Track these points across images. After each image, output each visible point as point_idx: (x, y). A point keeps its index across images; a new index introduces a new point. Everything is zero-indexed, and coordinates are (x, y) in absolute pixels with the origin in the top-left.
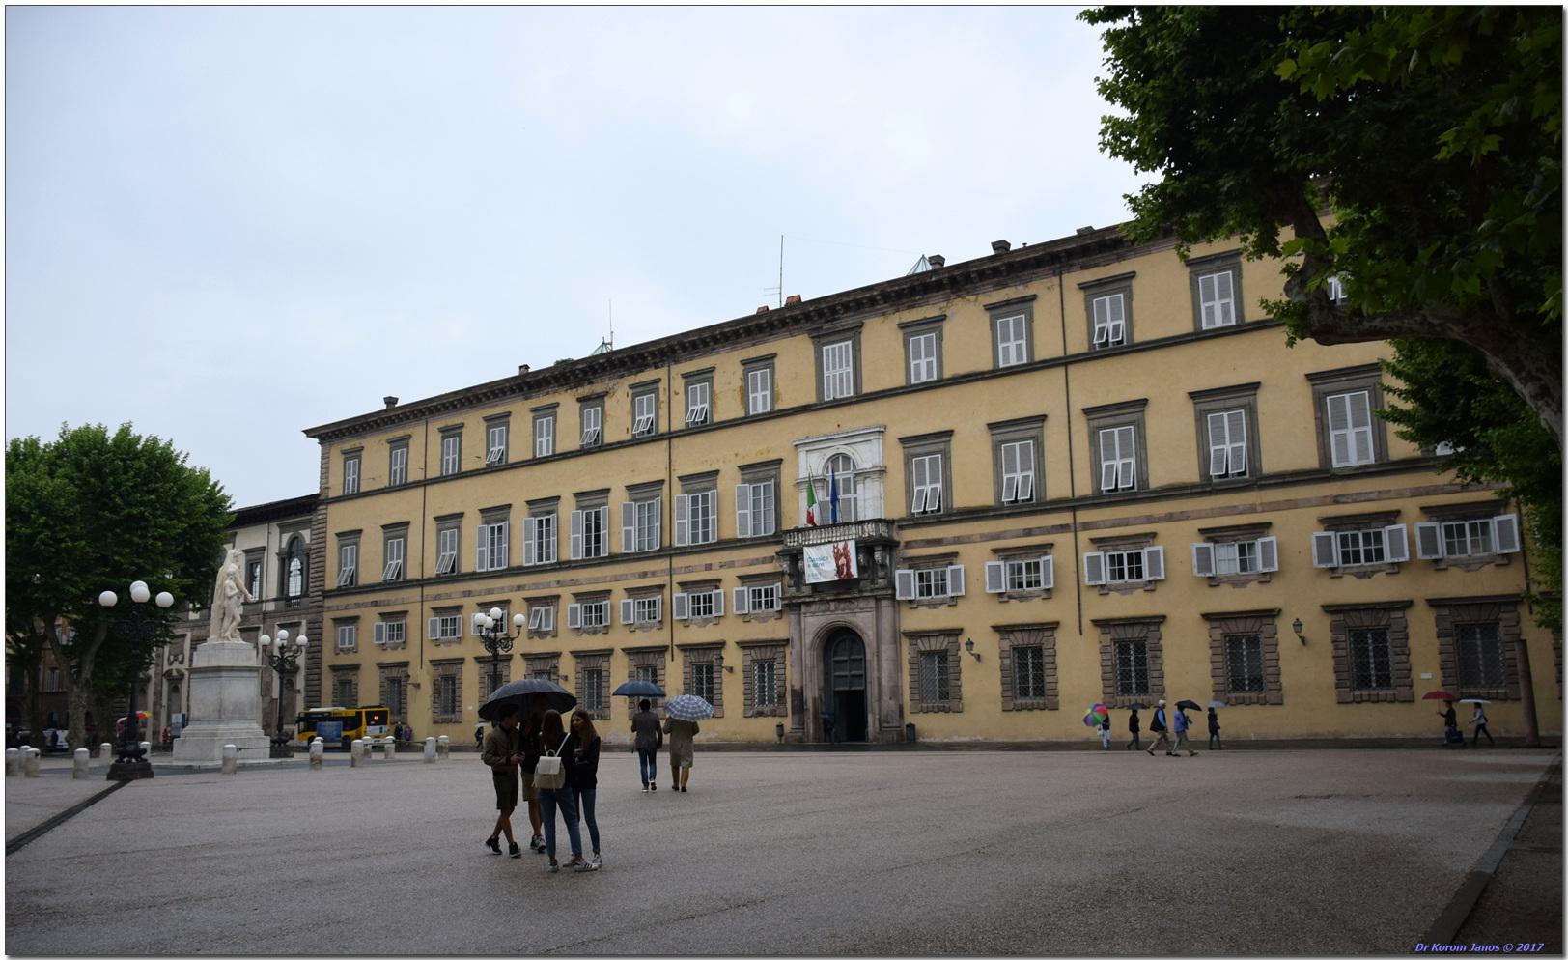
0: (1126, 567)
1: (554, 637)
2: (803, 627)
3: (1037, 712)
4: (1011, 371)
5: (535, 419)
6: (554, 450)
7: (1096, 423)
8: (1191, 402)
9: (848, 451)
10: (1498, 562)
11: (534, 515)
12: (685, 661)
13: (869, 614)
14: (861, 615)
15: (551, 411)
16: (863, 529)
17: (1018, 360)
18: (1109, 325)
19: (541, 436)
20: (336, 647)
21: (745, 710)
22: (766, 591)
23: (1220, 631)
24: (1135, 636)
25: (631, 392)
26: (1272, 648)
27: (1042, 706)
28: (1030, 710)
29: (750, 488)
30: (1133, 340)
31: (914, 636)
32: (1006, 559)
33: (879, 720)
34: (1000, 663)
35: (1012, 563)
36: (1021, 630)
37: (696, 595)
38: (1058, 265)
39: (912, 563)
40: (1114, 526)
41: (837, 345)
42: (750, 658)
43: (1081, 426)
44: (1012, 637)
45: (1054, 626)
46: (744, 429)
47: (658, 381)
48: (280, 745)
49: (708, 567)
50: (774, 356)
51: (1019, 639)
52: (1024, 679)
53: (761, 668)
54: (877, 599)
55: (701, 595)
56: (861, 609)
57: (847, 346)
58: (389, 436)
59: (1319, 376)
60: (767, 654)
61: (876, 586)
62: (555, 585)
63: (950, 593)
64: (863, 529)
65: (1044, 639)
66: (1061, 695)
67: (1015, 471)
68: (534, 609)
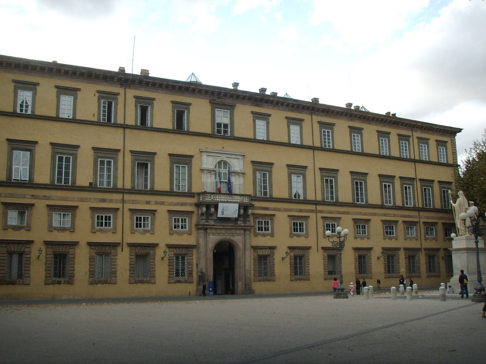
2: (208, 239)
3: (302, 281)
4: (295, 146)
6: (33, 111)
7: (323, 174)
9: (228, 160)
13: (241, 237)
22: (106, 217)
24: (19, 250)
25: (97, 95)
28: (300, 280)
31: (255, 248)
35: (294, 222)
36: (298, 249)
40: (328, 213)
43: (318, 173)
44: (294, 251)
45: (308, 248)
46: (377, 160)
47: (117, 94)
49: (148, 203)
51: (297, 252)
53: (177, 259)
54: (245, 230)
56: (238, 234)
59: (302, 167)
60: (184, 251)
62: (30, 197)
65: (306, 253)
66: (310, 275)
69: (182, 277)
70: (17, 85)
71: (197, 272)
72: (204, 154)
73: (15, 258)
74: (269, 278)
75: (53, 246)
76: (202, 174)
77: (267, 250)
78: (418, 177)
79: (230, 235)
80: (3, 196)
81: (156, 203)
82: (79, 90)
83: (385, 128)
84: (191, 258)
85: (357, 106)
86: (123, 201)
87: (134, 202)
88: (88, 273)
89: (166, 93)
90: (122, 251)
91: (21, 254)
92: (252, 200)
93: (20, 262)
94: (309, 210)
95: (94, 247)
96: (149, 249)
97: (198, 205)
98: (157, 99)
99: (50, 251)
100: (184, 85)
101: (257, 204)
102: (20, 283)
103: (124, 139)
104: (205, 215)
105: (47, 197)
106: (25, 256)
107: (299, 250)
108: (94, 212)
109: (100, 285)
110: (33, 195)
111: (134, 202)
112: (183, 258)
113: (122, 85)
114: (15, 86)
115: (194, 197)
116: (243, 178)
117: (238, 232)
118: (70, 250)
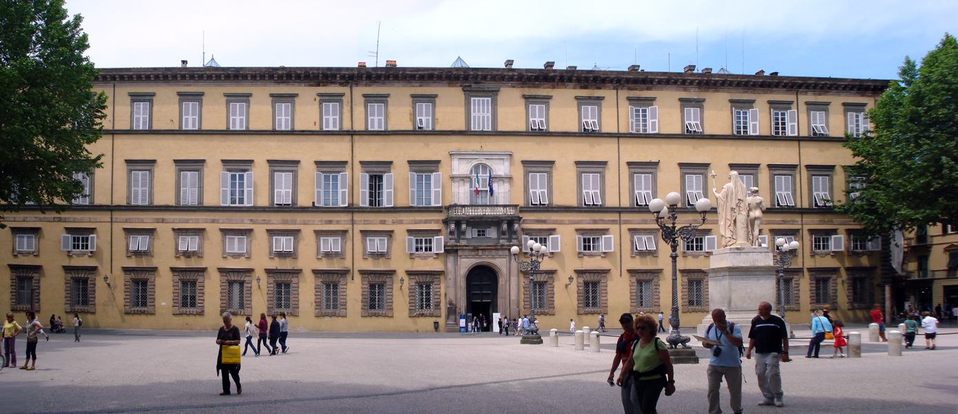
4: (303, 133)
6: (247, 127)
7: (633, 170)
8: (268, 165)
9: (488, 163)
13: (505, 259)
14: (499, 259)
20: (14, 250)
22: (83, 238)
23: (414, 281)
25: (318, 99)
27: (195, 313)
28: (592, 314)
29: (229, 174)
30: (152, 127)
32: (583, 234)
41: (481, 99)
43: (625, 170)
44: (584, 276)
47: (342, 95)
48: (532, 334)
49: (383, 222)
50: (436, 96)
51: (588, 277)
52: (587, 298)
53: (421, 287)
55: (81, 237)
57: (488, 101)
58: (685, 95)
61: (458, 244)
70: (230, 98)
71: (446, 303)
73: (236, 288)
78: (804, 163)
80: (221, 221)
81: (393, 223)
82: (296, 95)
83: (747, 94)
84: (438, 286)
85: (707, 69)
86: (353, 222)
87: (366, 222)
88: (314, 304)
89: (404, 86)
91: (242, 284)
92: (521, 211)
93: (241, 292)
95: (320, 276)
96: (385, 277)
97: (446, 222)
98: (158, 93)
99: (272, 280)
100: (426, 73)
101: (526, 216)
103: (352, 148)
104: (507, 233)
106: (245, 285)
107: (592, 275)
109: (327, 319)
111: (366, 222)
112: (428, 287)
113: (341, 84)
114: (227, 100)
115: (441, 212)
116: (510, 184)
117: (500, 253)
118: (387, 280)
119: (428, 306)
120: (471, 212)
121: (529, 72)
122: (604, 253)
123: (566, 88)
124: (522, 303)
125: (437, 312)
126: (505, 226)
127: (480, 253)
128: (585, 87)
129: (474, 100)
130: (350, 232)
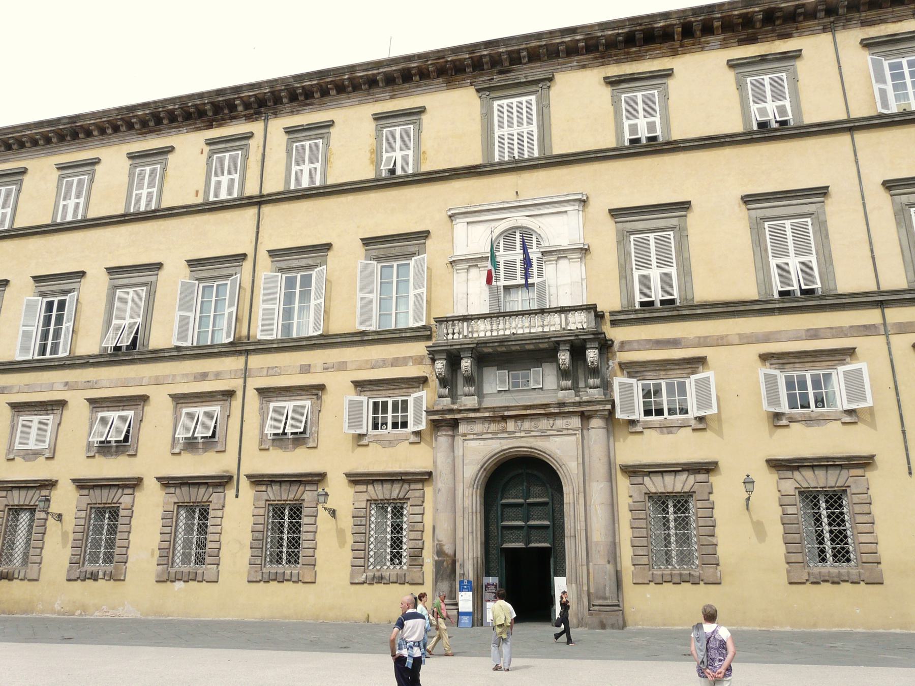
0: (811, 392)
1: (47, 458)
5: (61, 178)
10: (411, 441)
11: (43, 295)
12: (256, 499)
13: (573, 438)
15: (89, 168)
16: (566, 319)
17: (228, 194)
18: (398, 155)
19: (300, 162)
21: (352, 575)
25: (207, 149)
26: (865, 508)
31: (633, 471)
32: (782, 367)
33: (589, 595)
34: (780, 513)
37: (380, 400)
38: (832, 19)
39: (633, 369)
41: (514, 101)
42: (365, 497)
45: (865, 462)
47: (249, 136)
54: (585, 417)
57: (529, 103)
60: (395, 491)
61: (455, 407)
62: (61, 387)
63: (694, 411)
64: (566, 319)
67: (650, 267)
68: (100, 414)
69: (392, 567)
72: (458, 221)
74: (696, 574)
75: (91, 491)
76: (455, 273)
77: (683, 477)
79: (533, 434)
87: (271, 372)
88: (157, 553)
89: (360, 103)
90: (237, 496)
94: (851, 327)
102: (20, 578)
105: (91, 384)
108: (180, 405)
109: (179, 585)
110: (68, 382)
112: (398, 512)
113: (249, 118)
117: (560, 423)
119: (396, 557)
120: (483, 330)
121: (608, 29)
122: (850, 412)
123: (703, 49)
124: (626, 553)
125: (415, 574)
126: (564, 357)
127: (511, 425)
128: (752, 40)
129: (501, 107)
130: (239, 394)
